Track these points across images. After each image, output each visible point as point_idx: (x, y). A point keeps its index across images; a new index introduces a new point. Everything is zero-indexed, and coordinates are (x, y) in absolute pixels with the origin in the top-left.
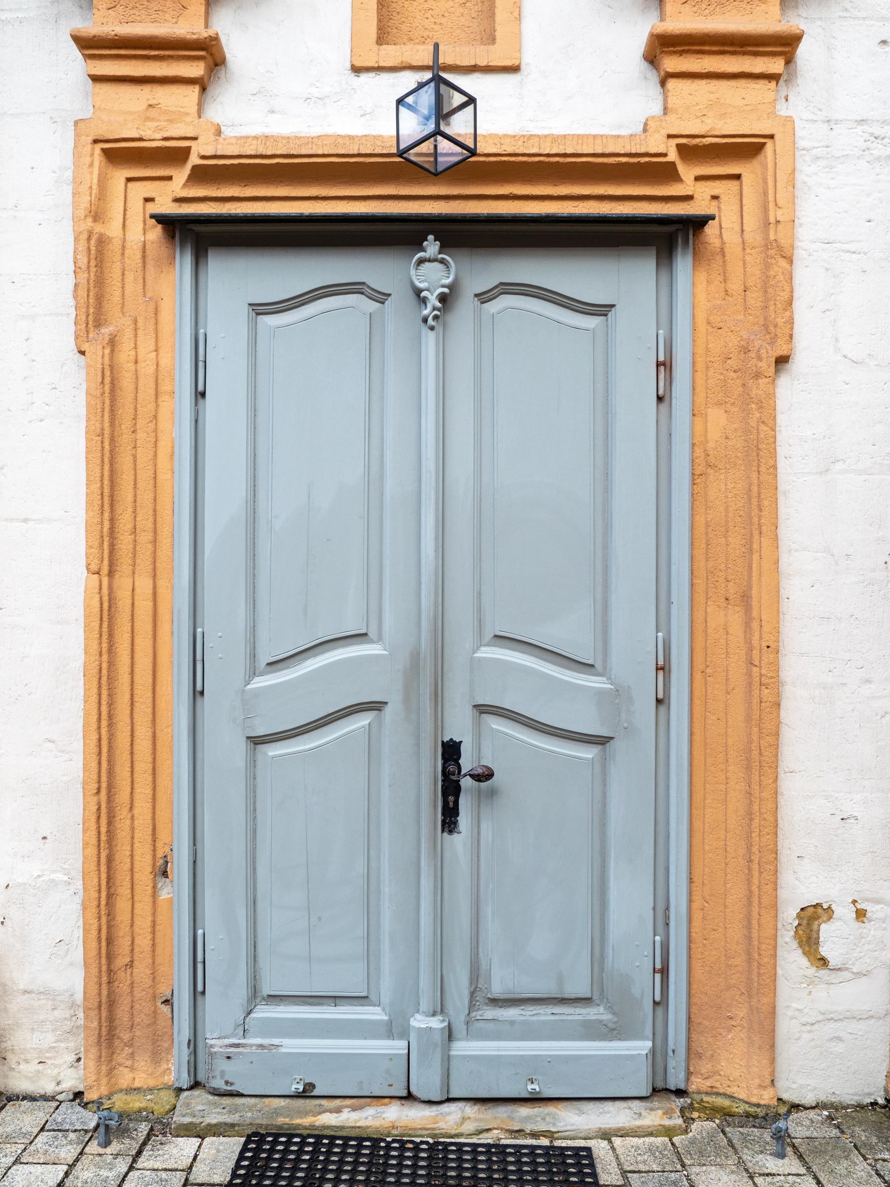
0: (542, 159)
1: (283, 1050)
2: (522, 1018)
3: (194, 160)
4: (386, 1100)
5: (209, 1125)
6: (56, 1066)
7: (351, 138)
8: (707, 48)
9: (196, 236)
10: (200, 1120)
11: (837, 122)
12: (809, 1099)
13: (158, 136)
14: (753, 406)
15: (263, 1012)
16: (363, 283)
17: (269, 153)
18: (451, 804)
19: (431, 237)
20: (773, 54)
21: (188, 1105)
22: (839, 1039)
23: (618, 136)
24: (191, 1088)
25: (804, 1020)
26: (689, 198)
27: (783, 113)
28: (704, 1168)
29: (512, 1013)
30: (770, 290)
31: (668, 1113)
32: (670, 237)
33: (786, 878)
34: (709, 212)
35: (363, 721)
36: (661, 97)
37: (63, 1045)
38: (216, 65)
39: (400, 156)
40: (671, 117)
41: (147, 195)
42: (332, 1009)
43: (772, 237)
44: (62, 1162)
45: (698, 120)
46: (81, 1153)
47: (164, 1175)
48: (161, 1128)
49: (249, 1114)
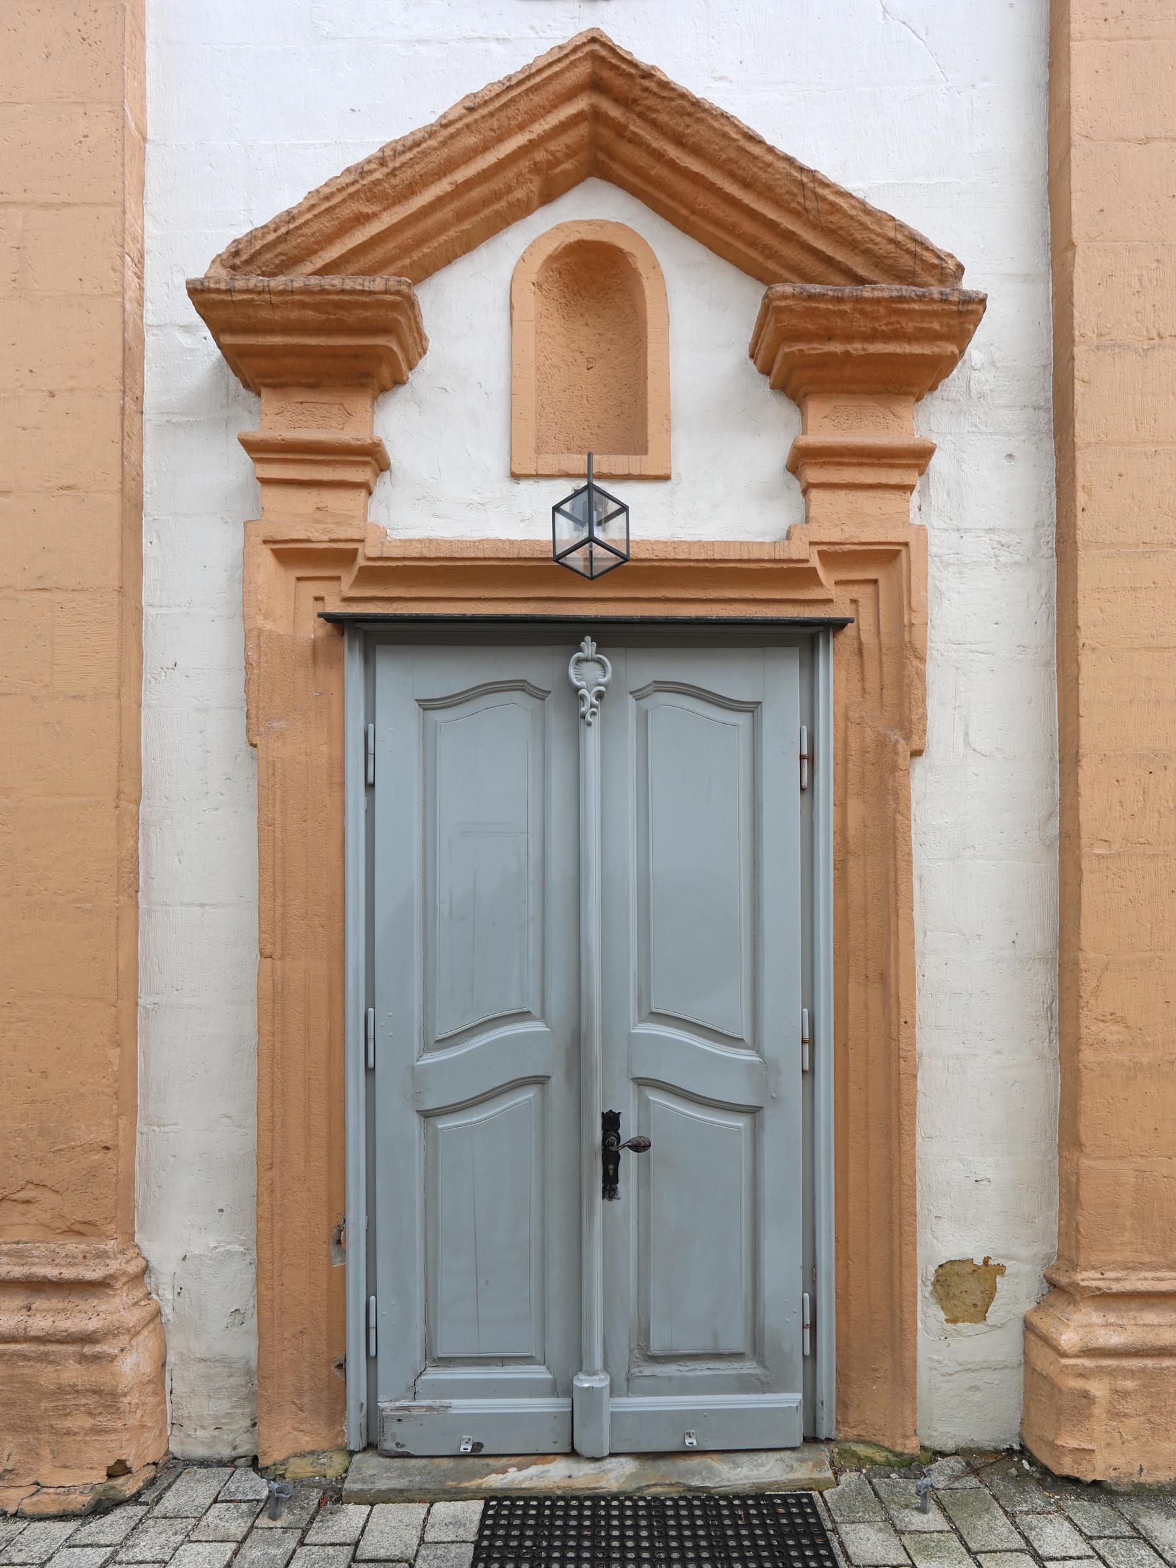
0: (691, 564)
1: (453, 1411)
2: (679, 1374)
3: (361, 562)
4: (551, 1457)
5: (379, 1491)
6: (232, 1431)
7: (511, 542)
8: (846, 460)
9: (366, 634)
10: (371, 1486)
11: (967, 530)
12: (950, 1446)
13: (326, 538)
14: (890, 797)
15: (435, 1375)
16: (525, 681)
17: (433, 556)
18: (611, 1172)
19: (588, 638)
20: (907, 466)
21: (359, 1469)
22: (976, 1388)
23: (763, 543)
24: (364, 1450)
25: (945, 1370)
26: (829, 601)
27: (917, 522)
28: (854, 1526)
29: (671, 1369)
30: (905, 689)
31: (818, 1465)
32: (809, 636)
33: (924, 1237)
34: (848, 615)
35: (529, 1094)
36: (803, 507)
37: (238, 1411)
38: (382, 470)
39: (557, 561)
40: (813, 526)
41: (317, 594)
42: (499, 1369)
43: (907, 638)
44: (231, 1538)
45: (838, 529)
46: (252, 1527)
47: (330, 1550)
48: (335, 1496)
49: (418, 1478)
